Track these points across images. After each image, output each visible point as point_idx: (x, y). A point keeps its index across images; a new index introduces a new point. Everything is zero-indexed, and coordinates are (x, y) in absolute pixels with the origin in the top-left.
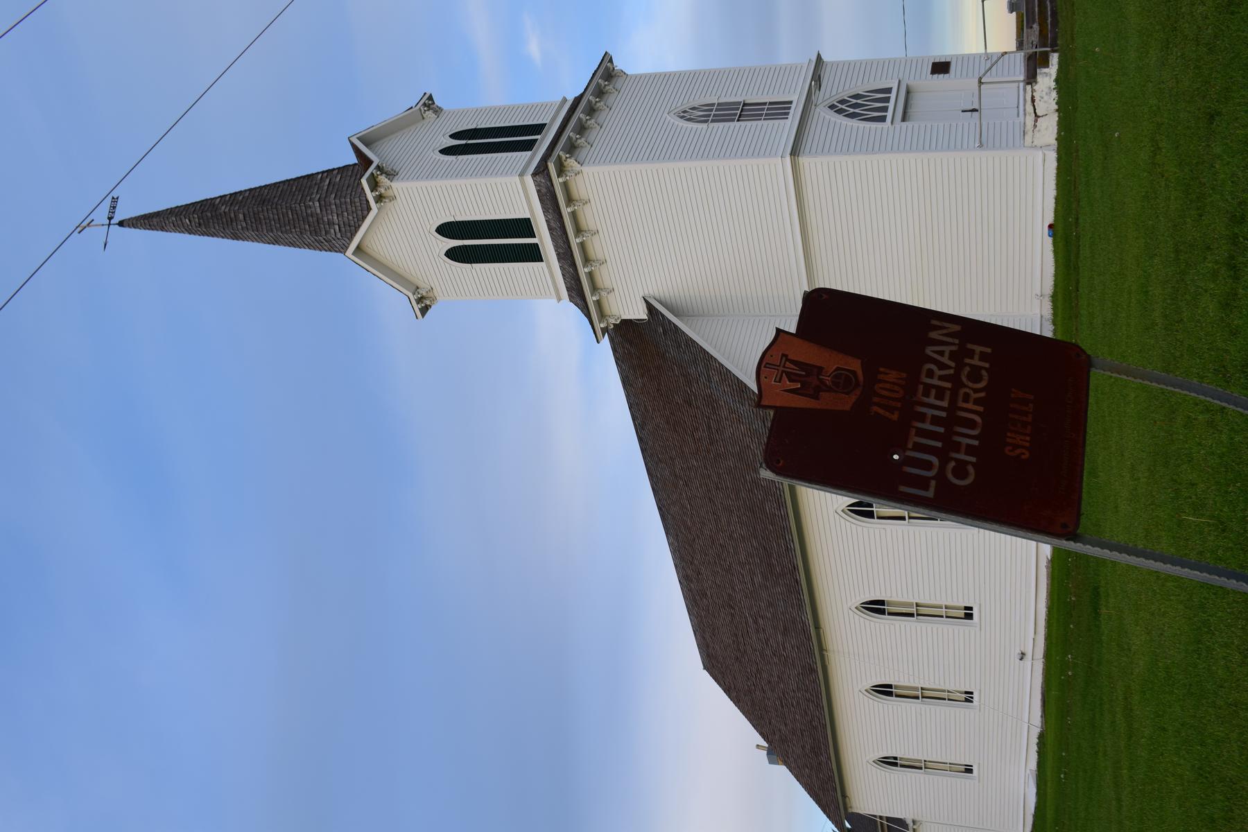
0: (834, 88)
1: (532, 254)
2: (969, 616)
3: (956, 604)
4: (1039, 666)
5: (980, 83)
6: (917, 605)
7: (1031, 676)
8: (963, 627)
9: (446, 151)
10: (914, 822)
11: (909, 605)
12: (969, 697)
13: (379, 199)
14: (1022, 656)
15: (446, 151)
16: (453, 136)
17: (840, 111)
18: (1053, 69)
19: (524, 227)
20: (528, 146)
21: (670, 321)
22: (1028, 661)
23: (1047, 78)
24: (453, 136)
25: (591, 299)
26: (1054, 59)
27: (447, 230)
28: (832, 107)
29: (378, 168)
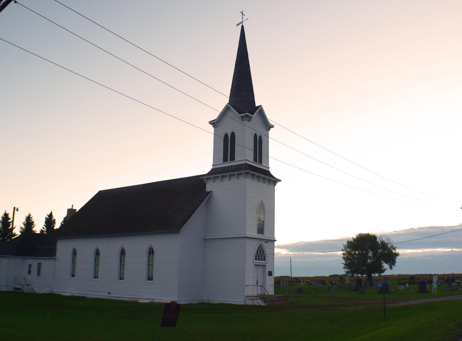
0: (266, 246)
1: (225, 160)
2: (121, 279)
3: (154, 274)
4: (107, 298)
5: (261, 286)
6: (124, 265)
7: (103, 295)
8: (145, 276)
9: (256, 135)
10: (55, 259)
11: (124, 262)
12: (150, 278)
13: (242, 117)
14: (109, 293)
15: (256, 135)
16: (260, 136)
17: (259, 248)
18: (263, 304)
19: (233, 158)
20: (255, 160)
21: (204, 199)
22: (107, 295)
23: (261, 303)
24: (260, 136)
25: (212, 176)
26: (266, 305)
27: (233, 134)
28: (260, 245)
29: (251, 117)
